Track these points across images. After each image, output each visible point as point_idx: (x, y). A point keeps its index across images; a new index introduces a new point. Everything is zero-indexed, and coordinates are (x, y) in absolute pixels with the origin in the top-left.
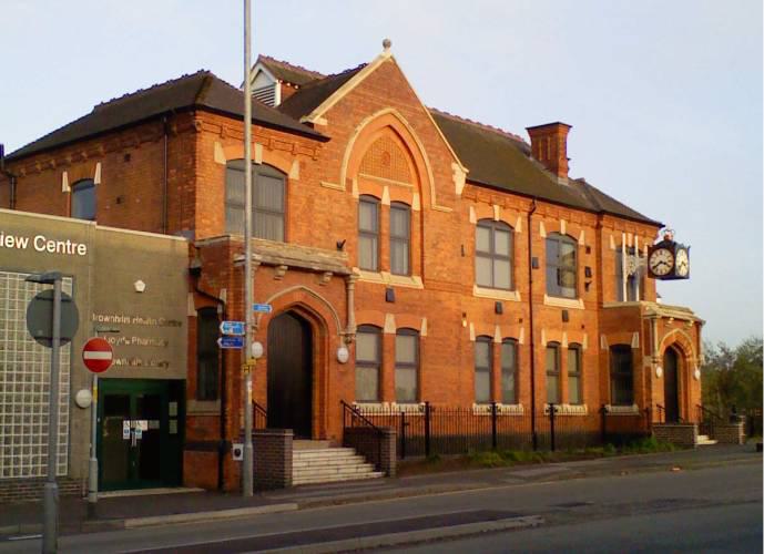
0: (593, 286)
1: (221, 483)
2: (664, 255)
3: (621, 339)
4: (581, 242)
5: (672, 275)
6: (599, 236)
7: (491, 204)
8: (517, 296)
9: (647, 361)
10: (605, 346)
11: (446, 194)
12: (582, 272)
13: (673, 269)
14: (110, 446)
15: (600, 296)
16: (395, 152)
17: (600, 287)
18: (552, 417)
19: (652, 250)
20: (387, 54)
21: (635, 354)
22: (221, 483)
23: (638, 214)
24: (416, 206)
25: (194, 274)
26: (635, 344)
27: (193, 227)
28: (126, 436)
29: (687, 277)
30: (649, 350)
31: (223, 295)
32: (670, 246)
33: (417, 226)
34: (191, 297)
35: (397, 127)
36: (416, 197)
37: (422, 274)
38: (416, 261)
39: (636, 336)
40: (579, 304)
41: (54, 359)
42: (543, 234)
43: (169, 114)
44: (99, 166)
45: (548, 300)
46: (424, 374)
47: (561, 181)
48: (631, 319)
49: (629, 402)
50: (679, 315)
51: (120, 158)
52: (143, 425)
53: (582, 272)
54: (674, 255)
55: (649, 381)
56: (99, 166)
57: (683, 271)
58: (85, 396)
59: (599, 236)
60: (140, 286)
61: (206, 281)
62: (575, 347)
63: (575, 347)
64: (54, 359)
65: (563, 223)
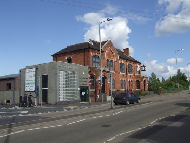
0: (134, 72)
1: (95, 101)
2: (143, 68)
3: (138, 79)
4: (132, 65)
5: (144, 70)
6: (134, 65)
7: (95, 53)
8: (125, 74)
9: (142, 83)
10: (135, 81)
11: (117, 58)
12: (132, 70)
13: (145, 69)
14: (81, 96)
15: (135, 73)
16: (111, 54)
17: (134, 72)
18: (132, 91)
19: (141, 67)
20: (110, 39)
21: (140, 82)
22: (95, 101)
23: (136, 60)
24: (113, 61)
25: (90, 72)
26: (140, 80)
27: (89, 65)
28: (82, 95)
29: (146, 71)
30: (142, 81)
31: (95, 74)
32: (143, 66)
33: (114, 64)
34: (89, 75)
35: (111, 50)
36: (113, 60)
37: (114, 71)
38: (114, 69)
39: (140, 79)
40: (132, 75)
41: (14, 94)
42: (128, 65)
43: (85, 49)
44: (72, 56)
45: (129, 74)
46: (115, 85)
47: (128, 57)
48: (139, 77)
49: (139, 89)
50: (145, 76)
51: (76, 55)
52: (84, 93)
53: (132, 70)
54: (145, 67)
55: (142, 86)
56: (72, 56)
57: (146, 70)
58: (79, 89)
59: (134, 65)
60: (83, 73)
61: (91, 73)
62: (132, 81)
63: (132, 81)
64: (14, 94)
65: (96, 53)
